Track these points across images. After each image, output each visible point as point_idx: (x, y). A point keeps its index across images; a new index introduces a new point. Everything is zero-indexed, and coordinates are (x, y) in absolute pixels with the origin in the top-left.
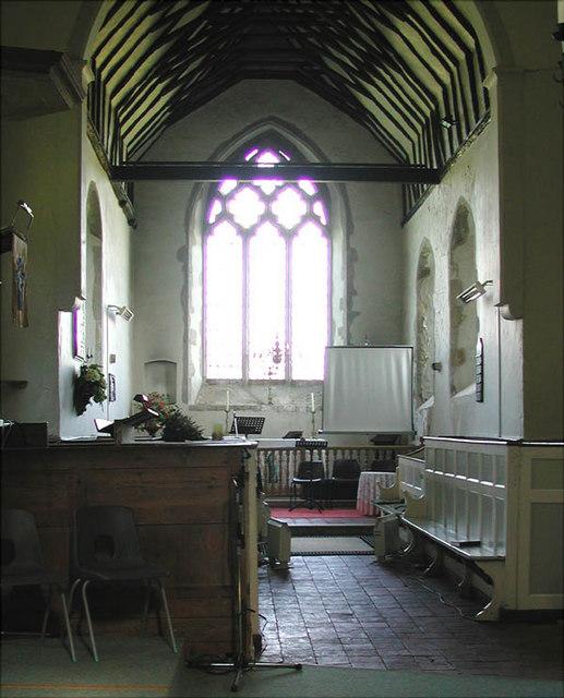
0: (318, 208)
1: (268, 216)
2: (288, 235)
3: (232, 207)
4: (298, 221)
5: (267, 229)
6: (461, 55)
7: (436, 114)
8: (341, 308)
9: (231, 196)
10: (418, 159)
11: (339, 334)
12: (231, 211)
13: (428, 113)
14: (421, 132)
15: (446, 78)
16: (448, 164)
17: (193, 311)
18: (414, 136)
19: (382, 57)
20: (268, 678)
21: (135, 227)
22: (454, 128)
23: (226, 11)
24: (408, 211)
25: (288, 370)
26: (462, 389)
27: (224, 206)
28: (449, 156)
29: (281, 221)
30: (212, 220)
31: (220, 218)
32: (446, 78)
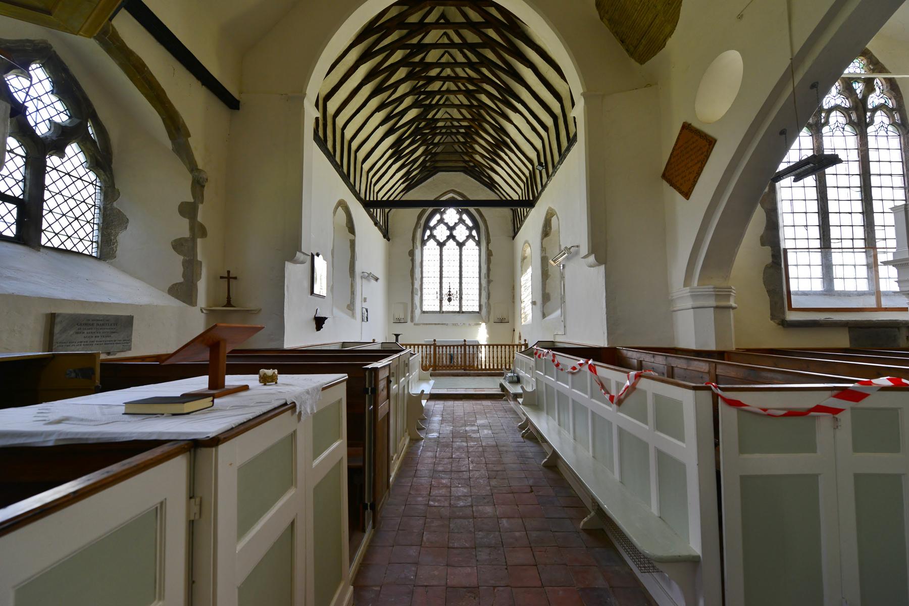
0: (474, 233)
1: (451, 237)
2: (461, 245)
3: (435, 232)
4: (465, 238)
5: (451, 243)
6: (548, 121)
7: (533, 174)
8: (485, 278)
9: (434, 227)
10: (491, 365)
11: (484, 290)
12: (434, 234)
13: (527, 173)
14: (523, 188)
15: (538, 144)
16: (540, 194)
17: (416, 280)
18: (522, 185)
19: (502, 143)
20: (9, 278)
21: (388, 240)
22: (544, 171)
23: (423, 90)
24: (516, 230)
25: (461, 306)
26: (549, 314)
27: (431, 232)
28: (540, 188)
29: (457, 238)
30: (426, 238)
31: (429, 237)
32: (538, 144)
